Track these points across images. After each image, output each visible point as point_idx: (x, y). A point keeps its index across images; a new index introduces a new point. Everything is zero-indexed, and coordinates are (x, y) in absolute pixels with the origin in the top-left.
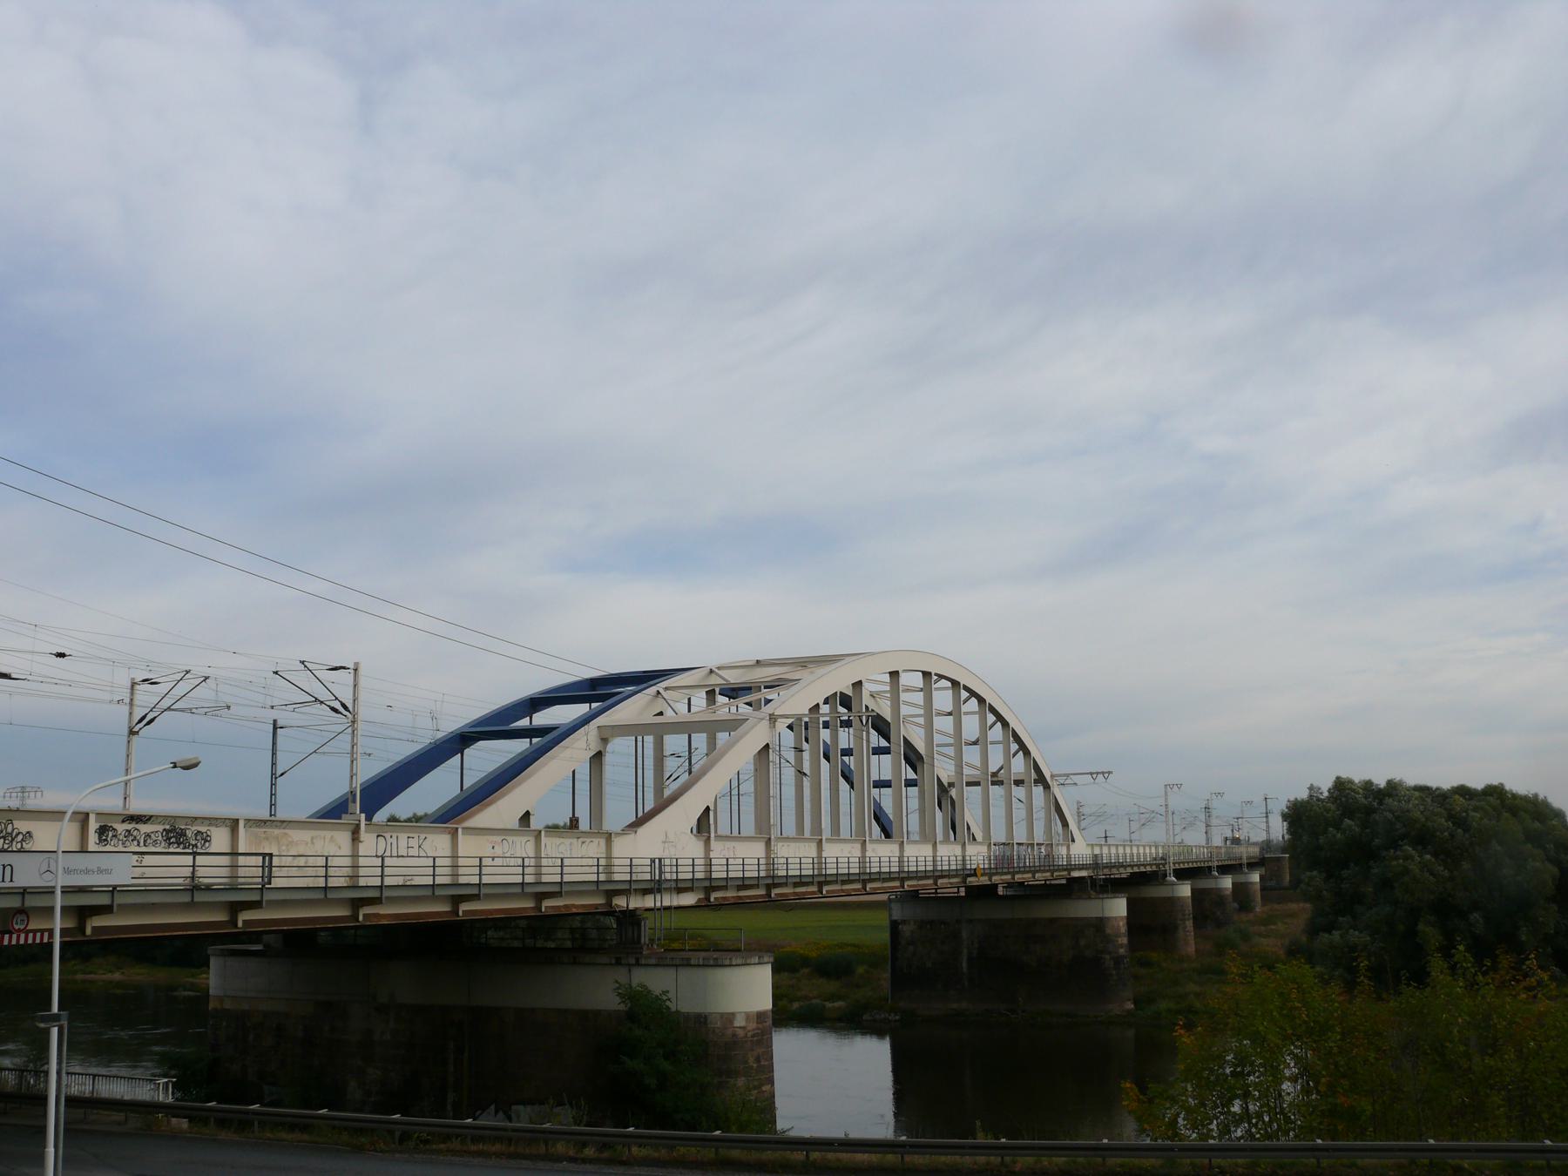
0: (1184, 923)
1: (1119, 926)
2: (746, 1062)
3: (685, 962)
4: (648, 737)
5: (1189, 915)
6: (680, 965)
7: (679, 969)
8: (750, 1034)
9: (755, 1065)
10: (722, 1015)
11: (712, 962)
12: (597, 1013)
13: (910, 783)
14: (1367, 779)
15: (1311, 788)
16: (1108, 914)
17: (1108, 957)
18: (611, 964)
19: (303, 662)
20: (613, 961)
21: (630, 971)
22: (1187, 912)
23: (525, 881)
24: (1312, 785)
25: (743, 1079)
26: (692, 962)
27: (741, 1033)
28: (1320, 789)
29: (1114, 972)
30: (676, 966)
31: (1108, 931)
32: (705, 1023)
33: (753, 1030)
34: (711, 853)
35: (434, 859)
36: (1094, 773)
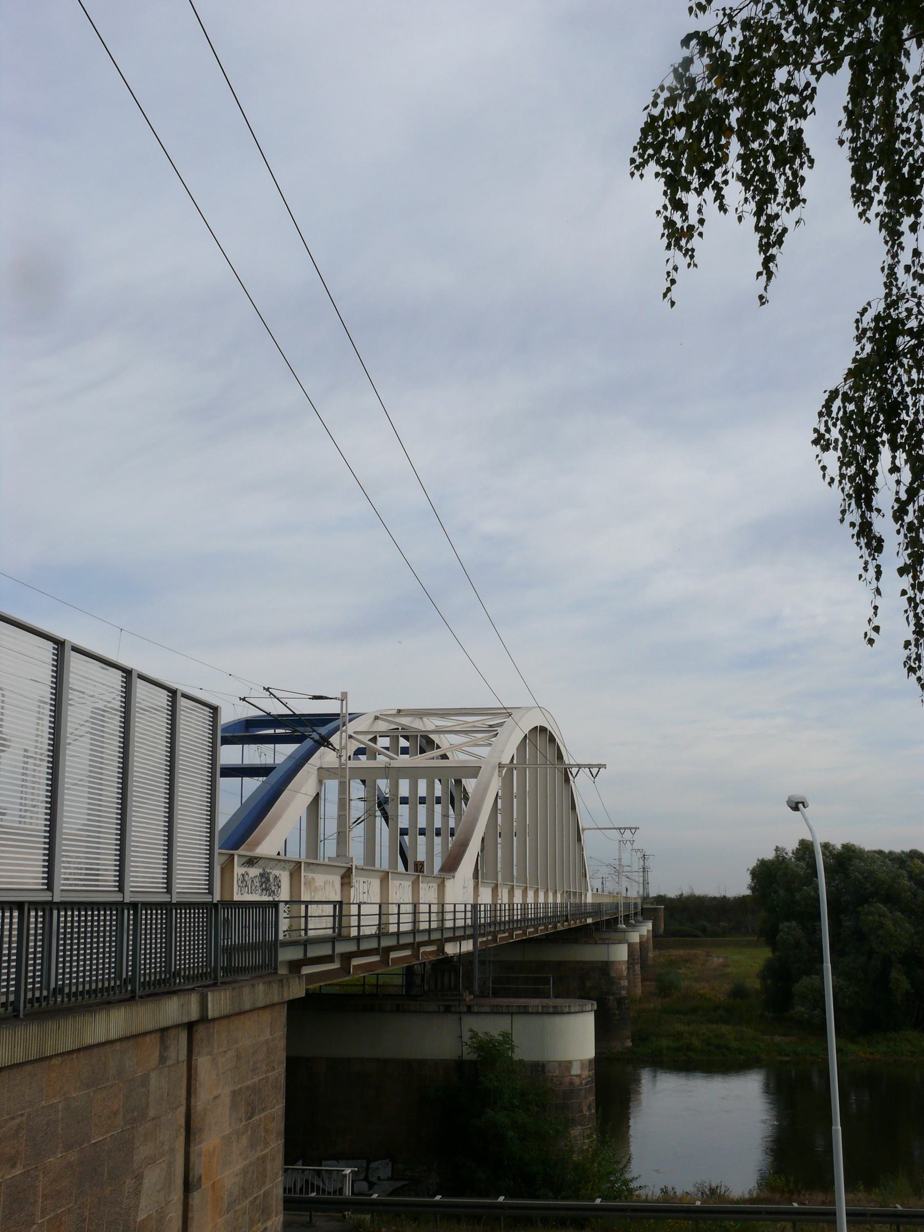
0: (634, 966)
1: (622, 970)
2: (581, 1111)
3: (522, 1010)
4: (331, 781)
5: (638, 959)
6: (515, 1013)
7: (515, 1017)
8: (584, 1082)
9: (588, 1114)
10: (560, 1063)
11: (551, 1010)
12: (422, 1063)
13: (404, 832)
14: (827, 841)
15: (777, 849)
16: (612, 958)
17: (611, 998)
18: (439, 1012)
19: (267, 689)
20: (442, 1009)
21: (460, 1018)
22: (636, 957)
23: (457, 925)
24: (777, 847)
25: (579, 1128)
26: (530, 1010)
27: (577, 1081)
28: (785, 849)
29: (617, 1012)
30: (512, 1014)
31: (613, 974)
32: (543, 1071)
33: (586, 1078)
34: (479, 898)
35: (430, 906)
36: (622, 828)
